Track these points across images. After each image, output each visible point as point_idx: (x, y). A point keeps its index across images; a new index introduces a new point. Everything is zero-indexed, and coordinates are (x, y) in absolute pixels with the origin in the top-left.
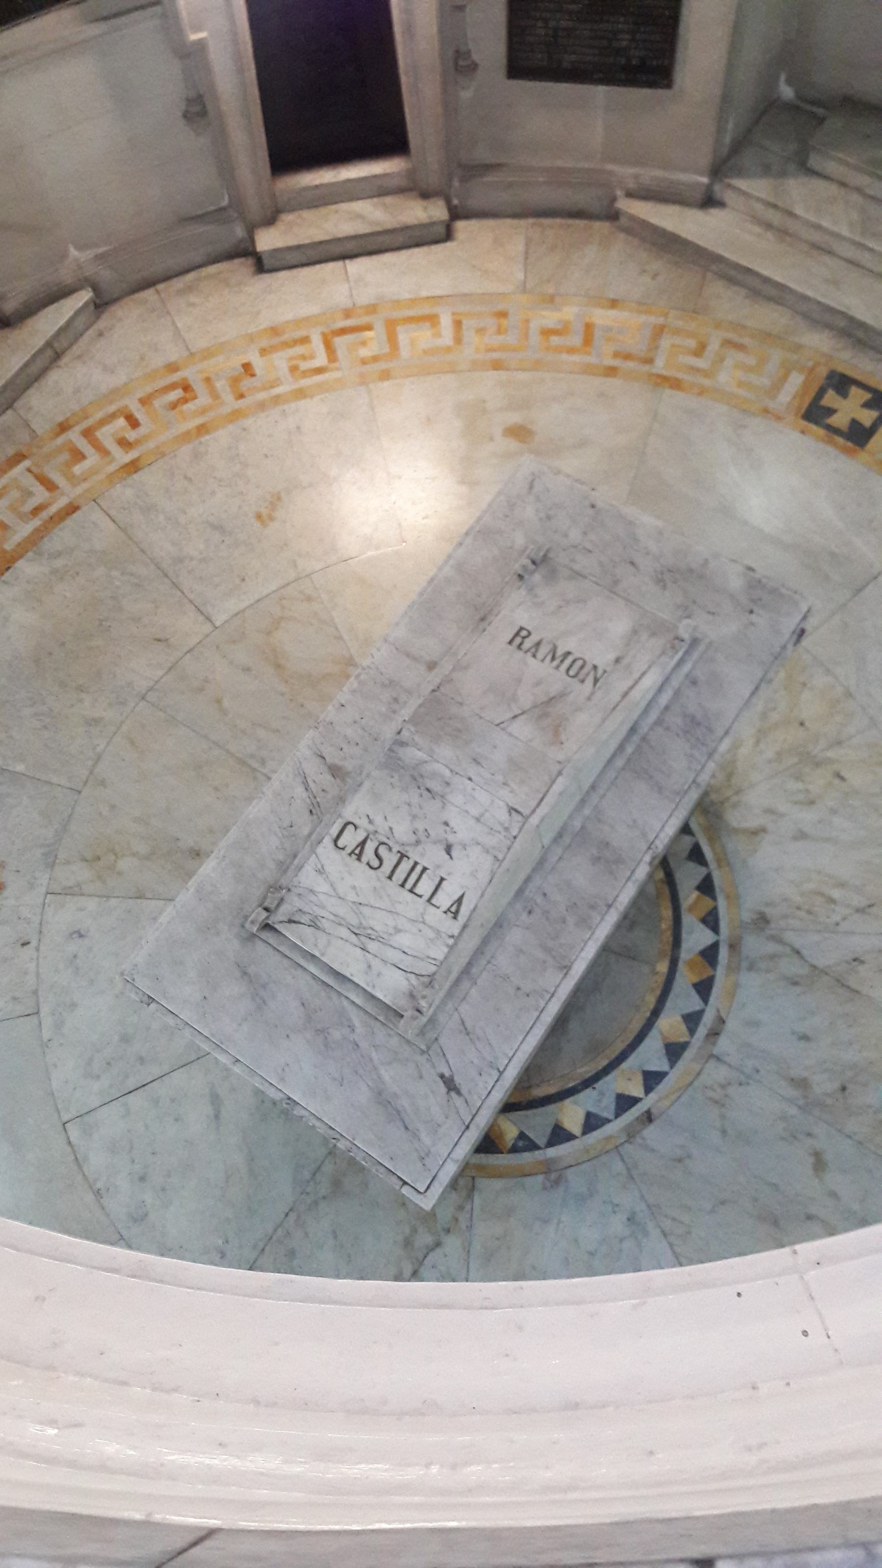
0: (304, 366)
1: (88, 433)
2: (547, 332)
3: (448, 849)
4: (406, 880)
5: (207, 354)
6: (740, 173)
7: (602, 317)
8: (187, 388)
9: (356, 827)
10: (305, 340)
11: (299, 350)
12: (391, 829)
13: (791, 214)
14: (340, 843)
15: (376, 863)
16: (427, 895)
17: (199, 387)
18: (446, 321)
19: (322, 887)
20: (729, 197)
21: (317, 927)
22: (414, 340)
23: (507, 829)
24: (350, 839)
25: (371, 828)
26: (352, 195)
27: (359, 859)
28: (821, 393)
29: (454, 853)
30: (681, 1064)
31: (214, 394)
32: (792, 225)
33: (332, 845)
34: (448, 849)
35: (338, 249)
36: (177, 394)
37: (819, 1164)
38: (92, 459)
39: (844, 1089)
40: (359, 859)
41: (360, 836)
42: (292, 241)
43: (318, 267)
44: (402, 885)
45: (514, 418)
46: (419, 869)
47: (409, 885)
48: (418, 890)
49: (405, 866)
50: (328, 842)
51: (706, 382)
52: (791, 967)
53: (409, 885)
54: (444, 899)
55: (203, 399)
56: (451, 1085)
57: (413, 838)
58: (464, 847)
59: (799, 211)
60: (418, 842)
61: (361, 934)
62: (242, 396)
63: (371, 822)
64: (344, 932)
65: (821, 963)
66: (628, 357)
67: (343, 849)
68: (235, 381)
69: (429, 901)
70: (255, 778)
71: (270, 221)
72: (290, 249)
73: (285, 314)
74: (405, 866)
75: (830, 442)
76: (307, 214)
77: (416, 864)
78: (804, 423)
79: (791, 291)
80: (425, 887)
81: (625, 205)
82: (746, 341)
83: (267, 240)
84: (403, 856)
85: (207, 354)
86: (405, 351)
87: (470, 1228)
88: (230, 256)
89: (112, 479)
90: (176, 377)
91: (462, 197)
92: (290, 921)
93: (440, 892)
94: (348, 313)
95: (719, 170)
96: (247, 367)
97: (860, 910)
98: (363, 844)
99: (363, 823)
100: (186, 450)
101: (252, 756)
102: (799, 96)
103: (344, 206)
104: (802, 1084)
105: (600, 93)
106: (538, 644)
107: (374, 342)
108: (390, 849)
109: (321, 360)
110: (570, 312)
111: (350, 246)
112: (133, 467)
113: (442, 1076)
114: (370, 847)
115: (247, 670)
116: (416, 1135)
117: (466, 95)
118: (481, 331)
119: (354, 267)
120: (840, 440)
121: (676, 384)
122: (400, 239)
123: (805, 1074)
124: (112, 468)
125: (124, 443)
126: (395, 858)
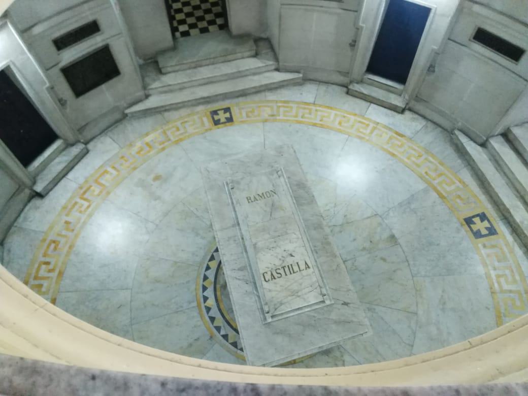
0: (83, 209)
1: (36, 278)
2: (138, 152)
3: (292, 255)
4: (290, 272)
5: (51, 228)
6: (149, 85)
7: (148, 139)
8: (54, 242)
9: (266, 273)
10: (76, 203)
11: (76, 207)
12: (274, 264)
13: (170, 85)
14: (267, 280)
15: (279, 275)
16: (298, 270)
17: (58, 239)
18: (109, 169)
19: (274, 294)
20: (151, 92)
21: (283, 304)
22: (106, 180)
23: (298, 238)
24: (268, 277)
25: (270, 269)
26: (52, 159)
27: (275, 278)
28: (213, 118)
29: (293, 255)
30: (221, 338)
31: (65, 236)
32: (171, 88)
33: (265, 282)
34: (292, 255)
35: (61, 175)
36: (53, 245)
37: (384, 260)
38: (45, 284)
39: (371, 242)
40: (275, 278)
41: (269, 273)
42: (47, 182)
43: (59, 184)
44: (291, 273)
45: (152, 176)
46: (290, 266)
47: (292, 272)
48: (295, 271)
49: (287, 269)
50: (264, 283)
51: (187, 134)
52: (337, 229)
53: (292, 272)
54: (303, 267)
55: (63, 241)
56: (345, 304)
57: (281, 262)
58: (294, 251)
59: (170, 83)
60: (283, 261)
61: (295, 294)
62: (73, 230)
63: (268, 268)
64: (290, 298)
65: (340, 223)
66: (163, 143)
67: (269, 280)
68: (67, 229)
69: (300, 270)
70: (184, 313)
71: (34, 183)
72: (47, 185)
73: (63, 201)
74: (287, 269)
75: (226, 126)
76: (45, 172)
77: (288, 266)
78: (217, 126)
79: (185, 102)
80: (296, 268)
81: (127, 111)
82: (186, 120)
83: (39, 188)
84: (283, 268)
85: (51, 228)
86: (107, 184)
87: (345, 350)
88: (29, 200)
89: (57, 282)
90: (47, 242)
91: (83, 138)
92: (276, 309)
93: (300, 266)
94: (81, 188)
95: (145, 87)
96: (67, 223)
97: (335, 207)
98: (272, 274)
99: (267, 270)
100: (72, 257)
101: (177, 308)
102: (145, 60)
103: (52, 163)
104: (364, 249)
105: (103, 87)
106: (255, 197)
107: (96, 189)
108: (279, 269)
109: (86, 204)
110: (139, 144)
111: (64, 172)
112: (61, 274)
113: (343, 304)
114: (275, 274)
115: (152, 290)
116: (352, 322)
117: (68, 110)
118: (121, 164)
119: (70, 176)
120: (227, 124)
121: (181, 140)
122: (76, 161)
123: (362, 247)
124: (54, 280)
125: (50, 271)
126: (282, 270)
